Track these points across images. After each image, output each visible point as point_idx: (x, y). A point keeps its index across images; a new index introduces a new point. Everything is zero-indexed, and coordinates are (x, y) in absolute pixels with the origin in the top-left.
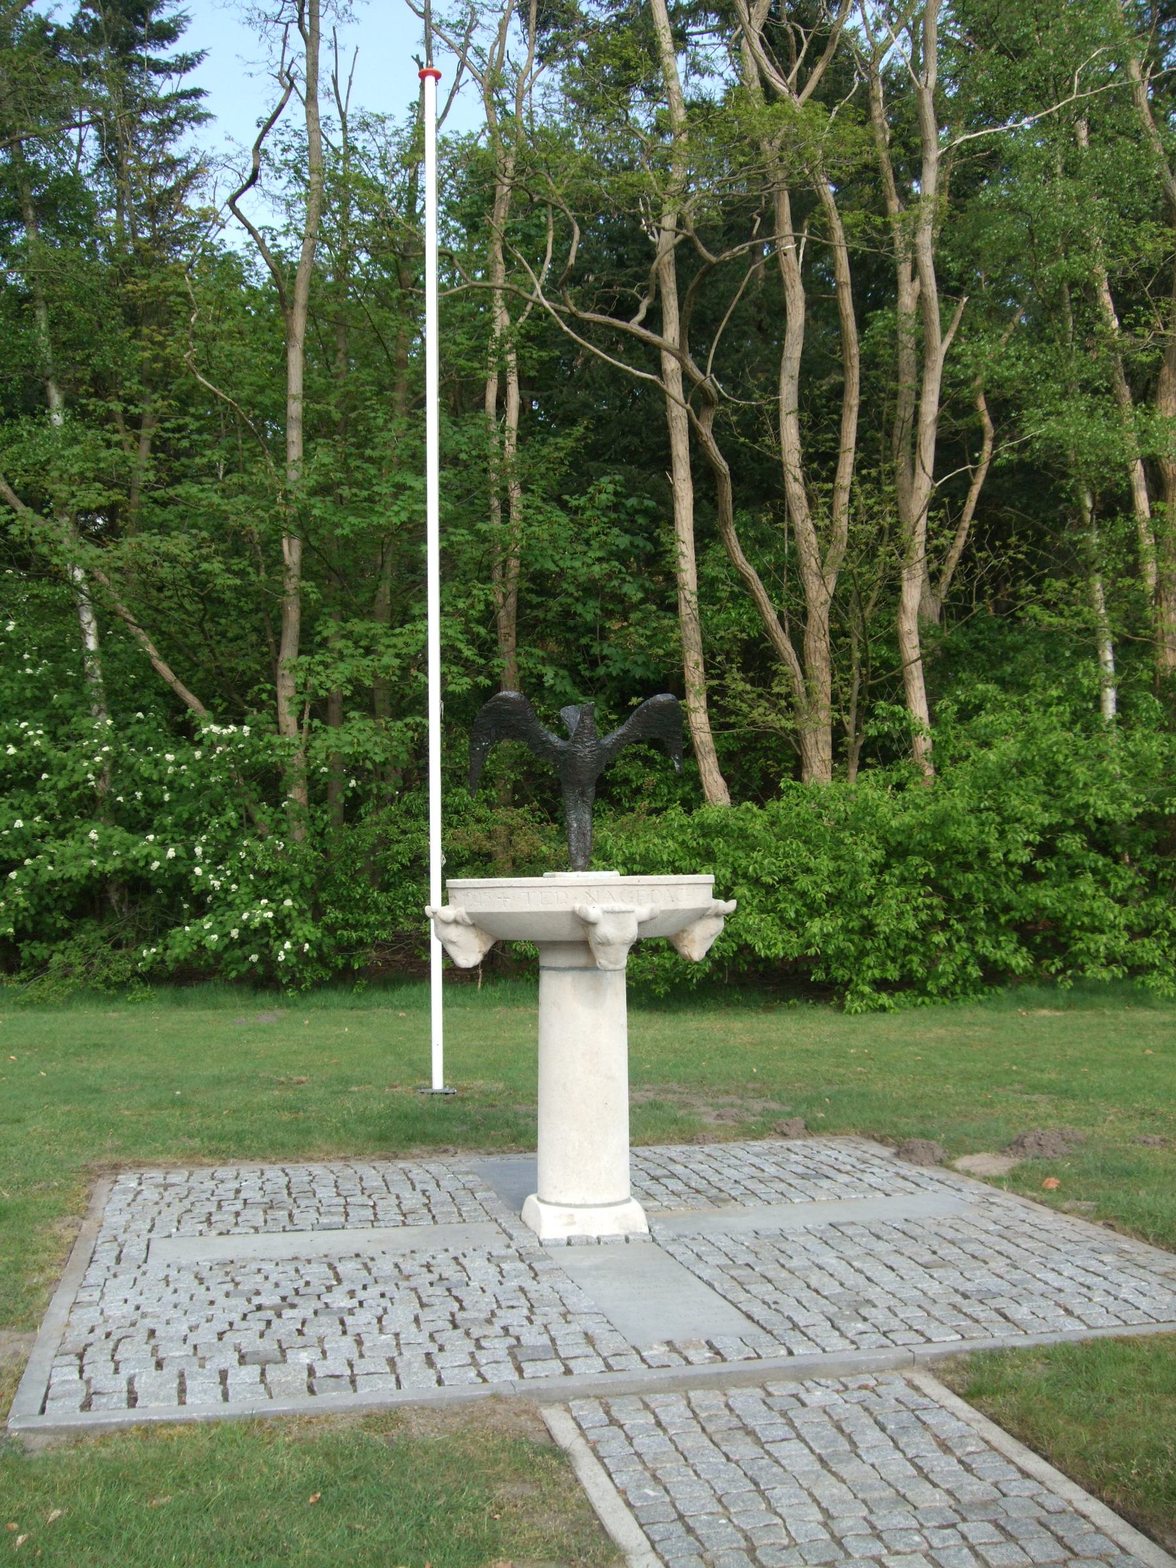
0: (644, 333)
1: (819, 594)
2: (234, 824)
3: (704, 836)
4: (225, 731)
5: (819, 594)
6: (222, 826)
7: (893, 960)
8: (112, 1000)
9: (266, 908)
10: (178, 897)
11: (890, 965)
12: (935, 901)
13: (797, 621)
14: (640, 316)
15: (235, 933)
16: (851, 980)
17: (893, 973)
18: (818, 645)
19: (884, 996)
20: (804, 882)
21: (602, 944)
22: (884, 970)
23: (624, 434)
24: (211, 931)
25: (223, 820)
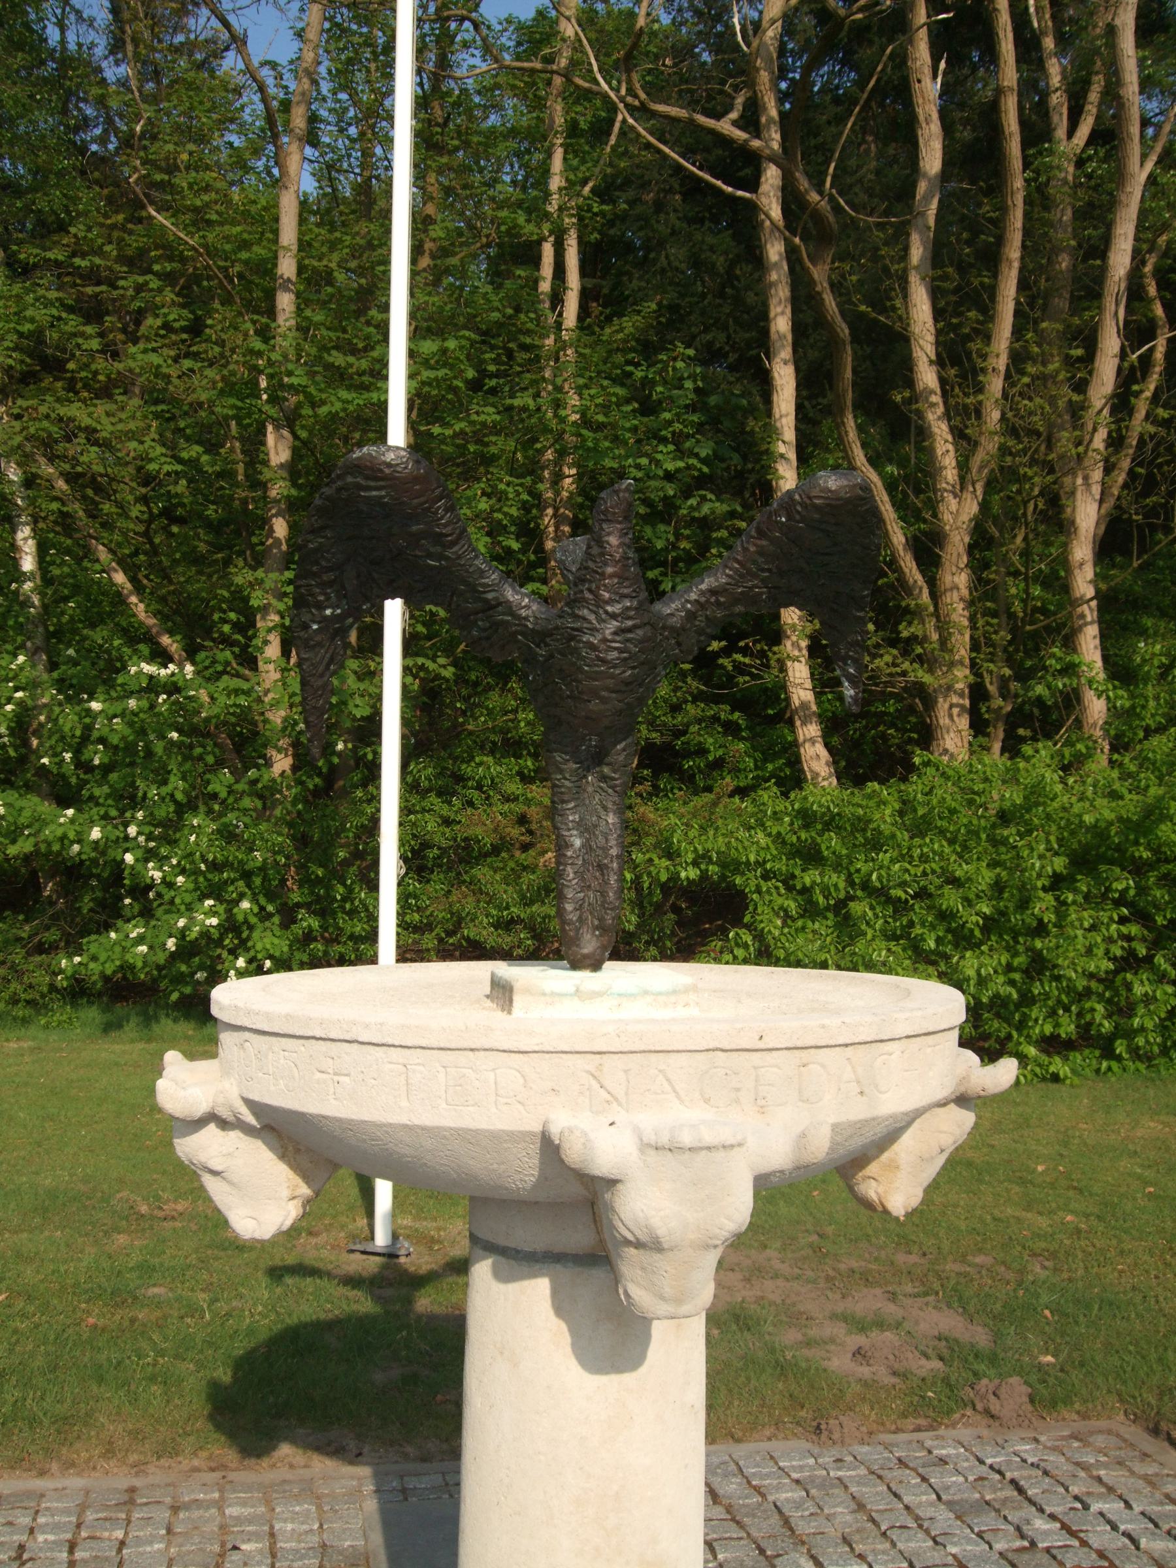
0: (740, 135)
1: (958, 513)
2: (179, 796)
3: (806, 826)
4: (163, 672)
5: (958, 513)
6: (163, 799)
7: (1067, 1009)
8: (25, 1021)
9: (212, 913)
10: (105, 893)
11: (1064, 1019)
12: (1134, 929)
13: (928, 550)
14: (734, 115)
15: (171, 944)
16: (1009, 1037)
17: (1068, 1028)
18: (957, 578)
19: (1057, 1059)
20: (950, 899)
21: (639, 1245)
22: (1057, 1025)
23: (706, 330)
24: (140, 940)
25: (168, 789)
